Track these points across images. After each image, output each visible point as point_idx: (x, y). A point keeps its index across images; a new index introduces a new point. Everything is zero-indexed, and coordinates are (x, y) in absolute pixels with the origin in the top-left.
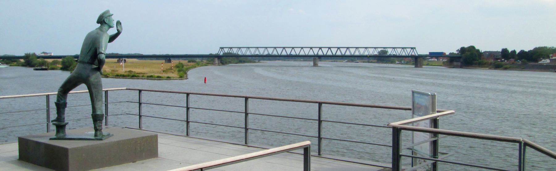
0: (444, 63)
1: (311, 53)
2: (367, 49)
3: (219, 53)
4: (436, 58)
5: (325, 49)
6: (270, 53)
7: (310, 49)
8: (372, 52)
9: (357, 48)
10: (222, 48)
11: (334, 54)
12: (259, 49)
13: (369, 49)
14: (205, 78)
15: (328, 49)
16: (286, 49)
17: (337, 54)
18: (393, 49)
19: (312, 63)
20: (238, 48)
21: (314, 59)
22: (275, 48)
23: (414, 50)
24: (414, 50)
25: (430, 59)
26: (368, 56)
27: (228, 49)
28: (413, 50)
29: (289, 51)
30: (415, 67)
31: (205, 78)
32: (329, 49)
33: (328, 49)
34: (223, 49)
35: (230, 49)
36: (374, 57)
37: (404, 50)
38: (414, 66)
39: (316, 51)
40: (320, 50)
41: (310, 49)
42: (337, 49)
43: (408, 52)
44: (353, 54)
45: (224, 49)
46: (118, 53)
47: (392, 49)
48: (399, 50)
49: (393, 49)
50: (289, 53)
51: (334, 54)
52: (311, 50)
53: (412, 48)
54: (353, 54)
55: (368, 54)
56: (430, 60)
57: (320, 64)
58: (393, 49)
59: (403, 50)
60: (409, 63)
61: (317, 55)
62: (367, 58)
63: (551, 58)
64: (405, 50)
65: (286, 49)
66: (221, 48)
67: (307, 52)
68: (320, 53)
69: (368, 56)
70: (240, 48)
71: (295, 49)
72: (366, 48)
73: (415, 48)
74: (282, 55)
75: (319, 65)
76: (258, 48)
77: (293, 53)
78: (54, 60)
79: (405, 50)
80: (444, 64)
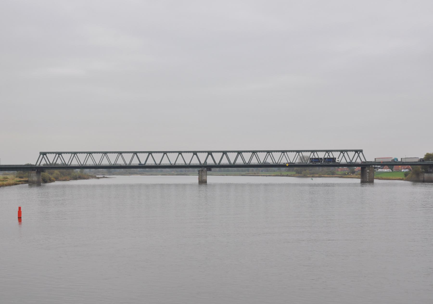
0: (406, 174)
1: (195, 162)
2: (285, 153)
3: (38, 163)
4: (390, 168)
5: (128, 154)
6: (143, 162)
7: (192, 154)
8: (293, 158)
9: (268, 152)
10: (44, 154)
11: (232, 162)
12: (108, 154)
13: (273, 153)
14: (20, 208)
15: (222, 154)
16: (138, 154)
17: (147, 163)
18: (342, 154)
19: (194, 179)
20: (56, 153)
21: (199, 171)
22: (135, 153)
23: (361, 154)
24: (361, 154)
25: (380, 168)
26: (287, 165)
27: (55, 154)
28: (359, 156)
29: (262, 157)
30: (363, 182)
31: (20, 208)
32: (210, 156)
33: (222, 154)
34: (45, 156)
35: (57, 155)
36: (292, 166)
37: (329, 154)
38: (359, 181)
39: (202, 157)
40: (195, 156)
41: (192, 154)
42: (148, 154)
43: (351, 157)
44: (247, 162)
45: (47, 155)
46: (28, 164)
47: (339, 153)
48: (351, 154)
49: (342, 154)
50: (203, 162)
51: (217, 162)
52: (180, 155)
53: (356, 151)
54: (97, 163)
55: (286, 162)
56: (379, 170)
57: (211, 179)
58: (298, 154)
59: (357, 154)
60: (348, 176)
61: (204, 164)
62: (284, 169)
63: (376, 171)
64: (346, 154)
65: (138, 154)
66: (41, 153)
67: (188, 159)
68: (210, 161)
69: (287, 165)
70: (60, 153)
71: (168, 154)
72: (283, 152)
73: (361, 151)
74: (161, 164)
75: (208, 181)
76: (90, 153)
77: (269, 161)
78: (227, 169)
79: (346, 154)
80: (407, 177)
